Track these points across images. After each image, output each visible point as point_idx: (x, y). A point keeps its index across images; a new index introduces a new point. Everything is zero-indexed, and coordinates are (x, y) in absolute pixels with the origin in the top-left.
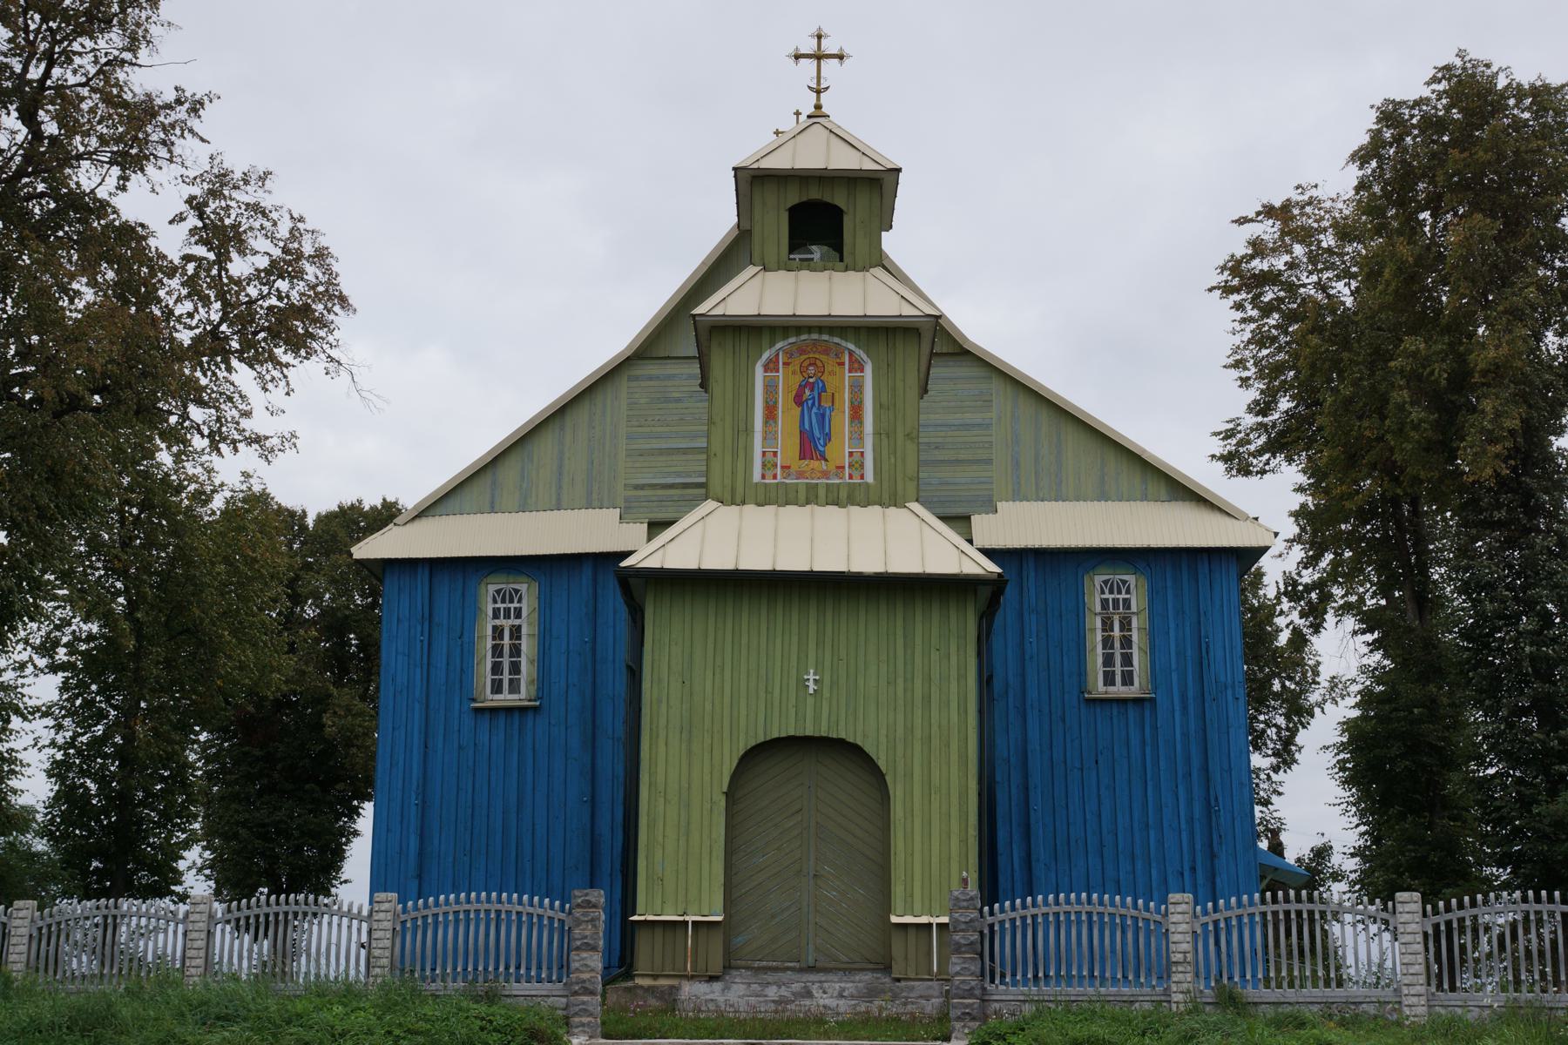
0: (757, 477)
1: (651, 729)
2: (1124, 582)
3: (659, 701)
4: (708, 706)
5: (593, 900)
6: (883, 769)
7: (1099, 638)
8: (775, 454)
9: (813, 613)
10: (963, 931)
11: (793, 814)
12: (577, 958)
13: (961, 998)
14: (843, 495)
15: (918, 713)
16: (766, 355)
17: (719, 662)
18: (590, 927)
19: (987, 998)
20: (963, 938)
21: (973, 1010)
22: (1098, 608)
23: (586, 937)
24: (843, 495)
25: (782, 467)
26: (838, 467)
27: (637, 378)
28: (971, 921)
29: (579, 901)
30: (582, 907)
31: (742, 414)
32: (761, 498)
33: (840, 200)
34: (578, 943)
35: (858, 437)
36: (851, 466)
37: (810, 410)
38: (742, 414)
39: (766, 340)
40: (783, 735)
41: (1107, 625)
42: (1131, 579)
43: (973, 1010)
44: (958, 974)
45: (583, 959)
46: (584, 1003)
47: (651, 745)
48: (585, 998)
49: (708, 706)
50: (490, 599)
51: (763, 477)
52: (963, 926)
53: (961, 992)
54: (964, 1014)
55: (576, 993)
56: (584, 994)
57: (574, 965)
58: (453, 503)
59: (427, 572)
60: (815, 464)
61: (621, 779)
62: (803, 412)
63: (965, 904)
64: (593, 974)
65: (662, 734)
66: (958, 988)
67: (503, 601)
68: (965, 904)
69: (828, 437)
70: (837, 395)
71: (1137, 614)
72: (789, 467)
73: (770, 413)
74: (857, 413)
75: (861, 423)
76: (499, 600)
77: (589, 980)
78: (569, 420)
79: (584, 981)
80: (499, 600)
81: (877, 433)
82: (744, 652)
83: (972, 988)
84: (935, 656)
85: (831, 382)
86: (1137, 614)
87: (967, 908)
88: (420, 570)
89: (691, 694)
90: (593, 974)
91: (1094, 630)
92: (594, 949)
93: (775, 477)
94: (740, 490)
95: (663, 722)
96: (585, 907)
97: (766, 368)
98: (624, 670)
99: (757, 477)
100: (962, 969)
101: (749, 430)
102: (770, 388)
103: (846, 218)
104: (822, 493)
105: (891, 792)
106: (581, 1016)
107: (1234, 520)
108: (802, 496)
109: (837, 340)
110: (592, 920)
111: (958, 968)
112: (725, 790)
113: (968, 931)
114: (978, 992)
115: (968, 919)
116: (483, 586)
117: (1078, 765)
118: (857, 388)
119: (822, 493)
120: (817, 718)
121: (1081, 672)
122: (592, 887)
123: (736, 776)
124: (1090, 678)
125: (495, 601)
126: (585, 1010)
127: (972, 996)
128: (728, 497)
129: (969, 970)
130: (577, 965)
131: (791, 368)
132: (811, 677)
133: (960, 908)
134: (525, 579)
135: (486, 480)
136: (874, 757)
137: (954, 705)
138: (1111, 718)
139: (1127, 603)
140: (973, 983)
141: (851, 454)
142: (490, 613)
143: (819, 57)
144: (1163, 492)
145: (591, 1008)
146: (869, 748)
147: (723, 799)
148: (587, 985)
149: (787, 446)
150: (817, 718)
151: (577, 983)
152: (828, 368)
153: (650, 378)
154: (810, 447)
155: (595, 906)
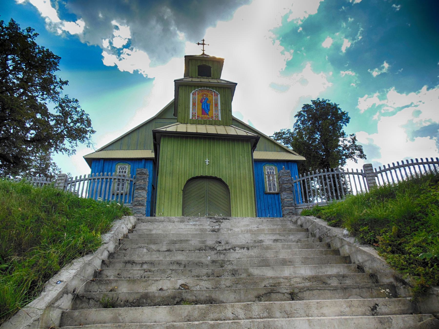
0: (191, 117)
1: (161, 173)
2: (272, 168)
3: (164, 166)
4: (178, 168)
5: (144, 172)
6: (228, 185)
7: (267, 180)
8: (195, 113)
9: (207, 143)
10: (286, 183)
11: (202, 198)
12: (137, 192)
13: (288, 207)
14: (213, 122)
15: (237, 171)
16: (193, 91)
17: (181, 157)
18: (143, 181)
19: (296, 208)
20: (286, 186)
21: (293, 211)
22: (267, 173)
23: (141, 185)
24: (213, 122)
25: (197, 116)
26: (212, 117)
27: (157, 122)
28: (289, 180)
29: (139, 172)
30: (140, 174)
31: (187, 104)
32: (192, 123)
33: (210, 65)
34: (138, 187)
35: (217, 110)
36: (215, 117)
37: (204, 104)
38: (187, 104)
39: (193, 88)
40: (199, 175)
41: (269, 177)
42: (274, 167)
43: (293, 211)
44: (286, 198)
45: (139, 193)
46: (139, 209)
47: (161, 177)
48: (139, 207)
49: (178, 168)
50: (118, 169)
51: (192, 118)
52: (286, 182)
53: (287, 205)
54: (289, 212)
55: (136, 205)
56: (139, 206)
57: (135, 195)
58: (110, 147)
59: (103, 162)
60: (206, 116)
61: (150, 212)
62: (202, 104)
63: (286, 174)
64: (143, 198)
65: (164, 174)
66: (286, 203)
67: (122, 169)
68: (286, 174)
69: (209, 110)
70: (211, 101)
71: (275, 175)
72: (199, 116)
73: (194, 104)
74: (216, 105)
75: (217, 107)
76: (120, 169)
77: (141, 200)
78: (140, 130)
79: (139, 201)
80: (120, 169)
81: (222, 110)
82: (188, 154)
83: (292, 203)
84: (241, 157)
85: (210, 98)
86: (275, 175)
87: (287, 176)
88: (101, 161)
89: (173, 165)
90: (143, 198)
91: (266, 178)
92: (144, 189)
93: (195, 118)
94: (186, 120)
95: (165, 171)
96: (141, 174)
97: (193, 94)
98: (151, 186)
99: (191, 117)
100: (287, 197)
101: (189, 108)
102: (194, 99)
103: (212, 69)
104: (208, 122)
105: (230, 191)
106: (137, 214)
107: (294, 155)
108: (203, 123)
109: (211, 89)
110: (143, 179)
111: (286, 196)
112: (183, 189)
113: (288, 184)
114: (294, 205)
115: (287, 180)
116: (117, 165)
117: (264, 208)
118: (216, 100)
119: (208, 122)
120: (209, 171)
121: (264, 188)
122: (145, 168)
123: (185, 186)
124: (266, 189)
125: (119, 169)
126: (139, 212)
127: (292, 206)
128: (183, 122)
129: (290, 197)
130: (137, 195)
131: (199, 95)
132: (207, 161)
133: (284, 176)
134: (127, 164)
135: (119, 142)
136: (225, 182)
137: (247, 169)
138: (271, 198)
139: (273, 172)
140: (292, 202)
141: (215, 114)
142: (118, 172)
143: (203, 44)
144: (279, 149)
145: (141, 211)
146: (224, 179)
147: (182, 191)
148: (140, 202)
149: (198, 112)
150: (209, 171)
151: (136, 202)
152: (209, 95)
153: (160, 123)
154: (204, 112)
155: (145, 174)
